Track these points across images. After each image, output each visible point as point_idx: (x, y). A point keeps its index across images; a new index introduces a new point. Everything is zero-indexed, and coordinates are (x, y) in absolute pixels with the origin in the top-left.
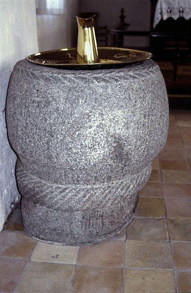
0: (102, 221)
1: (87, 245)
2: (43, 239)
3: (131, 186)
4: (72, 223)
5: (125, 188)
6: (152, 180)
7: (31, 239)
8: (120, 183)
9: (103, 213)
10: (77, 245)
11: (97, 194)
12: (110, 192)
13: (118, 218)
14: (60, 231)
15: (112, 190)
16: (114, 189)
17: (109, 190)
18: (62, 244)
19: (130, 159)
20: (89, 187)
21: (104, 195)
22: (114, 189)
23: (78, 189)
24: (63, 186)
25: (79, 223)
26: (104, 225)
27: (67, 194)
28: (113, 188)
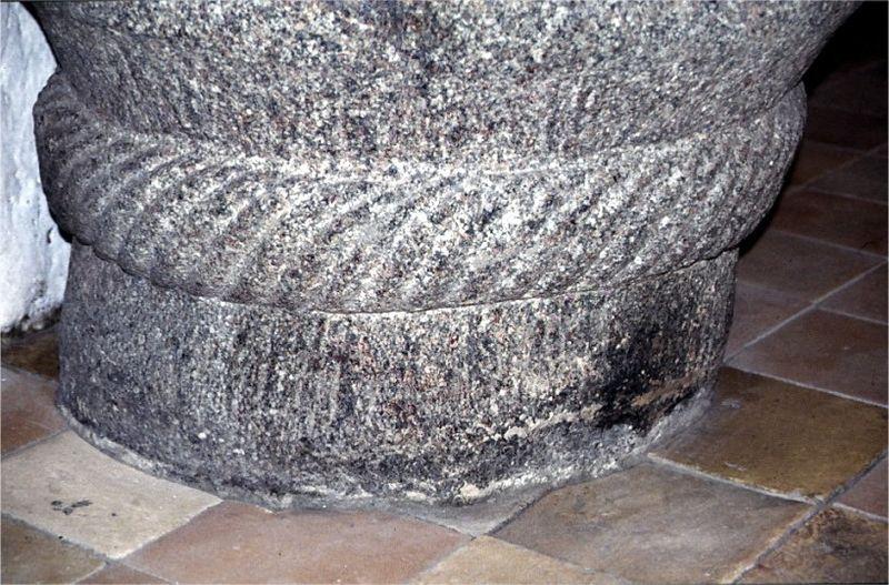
0: (344, 389)
1: (264, 504)
2: (85, 422)
3: (511, 218)
4: (186, 356)
5: (464, 214)
6: (880, 268)
7: (55, 412)
8: (434, 182)
9: (352, 339)
10: (213, 490)
11: (288, 209)
12: (360, 214)
13: (444, 396)
14: (137, 391)
15: (375, 208)
16: (392, 207)
17: (355, 204)
18: (150, 464)
19: (450, 30)
20: (257, 163)
21: (327, 221)
22: (392, 207)
23: (199, 167)
24: (146, 138)
25: (219, 365)
26: (350, 408)
27: (146, 181)
28: (389, 198)
